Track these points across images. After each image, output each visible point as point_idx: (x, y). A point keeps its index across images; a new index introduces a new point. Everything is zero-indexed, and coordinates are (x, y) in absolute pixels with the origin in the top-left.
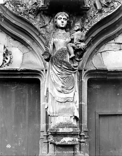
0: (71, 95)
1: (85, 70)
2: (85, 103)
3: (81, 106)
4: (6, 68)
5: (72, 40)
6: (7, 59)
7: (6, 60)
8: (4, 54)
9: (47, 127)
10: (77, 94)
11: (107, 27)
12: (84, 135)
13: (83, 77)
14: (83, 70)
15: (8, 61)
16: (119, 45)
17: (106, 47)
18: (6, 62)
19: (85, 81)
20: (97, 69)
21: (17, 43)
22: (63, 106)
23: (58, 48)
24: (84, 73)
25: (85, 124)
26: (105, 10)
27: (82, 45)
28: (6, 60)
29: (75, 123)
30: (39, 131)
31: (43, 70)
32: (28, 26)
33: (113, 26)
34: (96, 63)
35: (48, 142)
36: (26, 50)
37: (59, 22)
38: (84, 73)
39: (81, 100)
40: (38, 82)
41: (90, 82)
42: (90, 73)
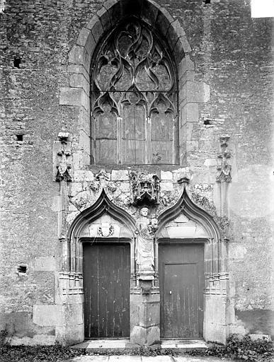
0: (150, 253)
2: (157, 257)
4: (111, 236)
5: (151, 223)
11: (86, 305)
17: (170, 224)
19: (157, 244)
21: (117, 222)
22: (146, 259)
23: (143, 228)
25: (157, 269)
26: (168, 204)
27: (156, 226)
29: (152, 269)
30: (130, 274)
33: (195, 214)
34: (164, 234)
36: (122, 226)
37: (143, 214)
38: (156, 240)
40: (129, 244)
42: (160, 240)
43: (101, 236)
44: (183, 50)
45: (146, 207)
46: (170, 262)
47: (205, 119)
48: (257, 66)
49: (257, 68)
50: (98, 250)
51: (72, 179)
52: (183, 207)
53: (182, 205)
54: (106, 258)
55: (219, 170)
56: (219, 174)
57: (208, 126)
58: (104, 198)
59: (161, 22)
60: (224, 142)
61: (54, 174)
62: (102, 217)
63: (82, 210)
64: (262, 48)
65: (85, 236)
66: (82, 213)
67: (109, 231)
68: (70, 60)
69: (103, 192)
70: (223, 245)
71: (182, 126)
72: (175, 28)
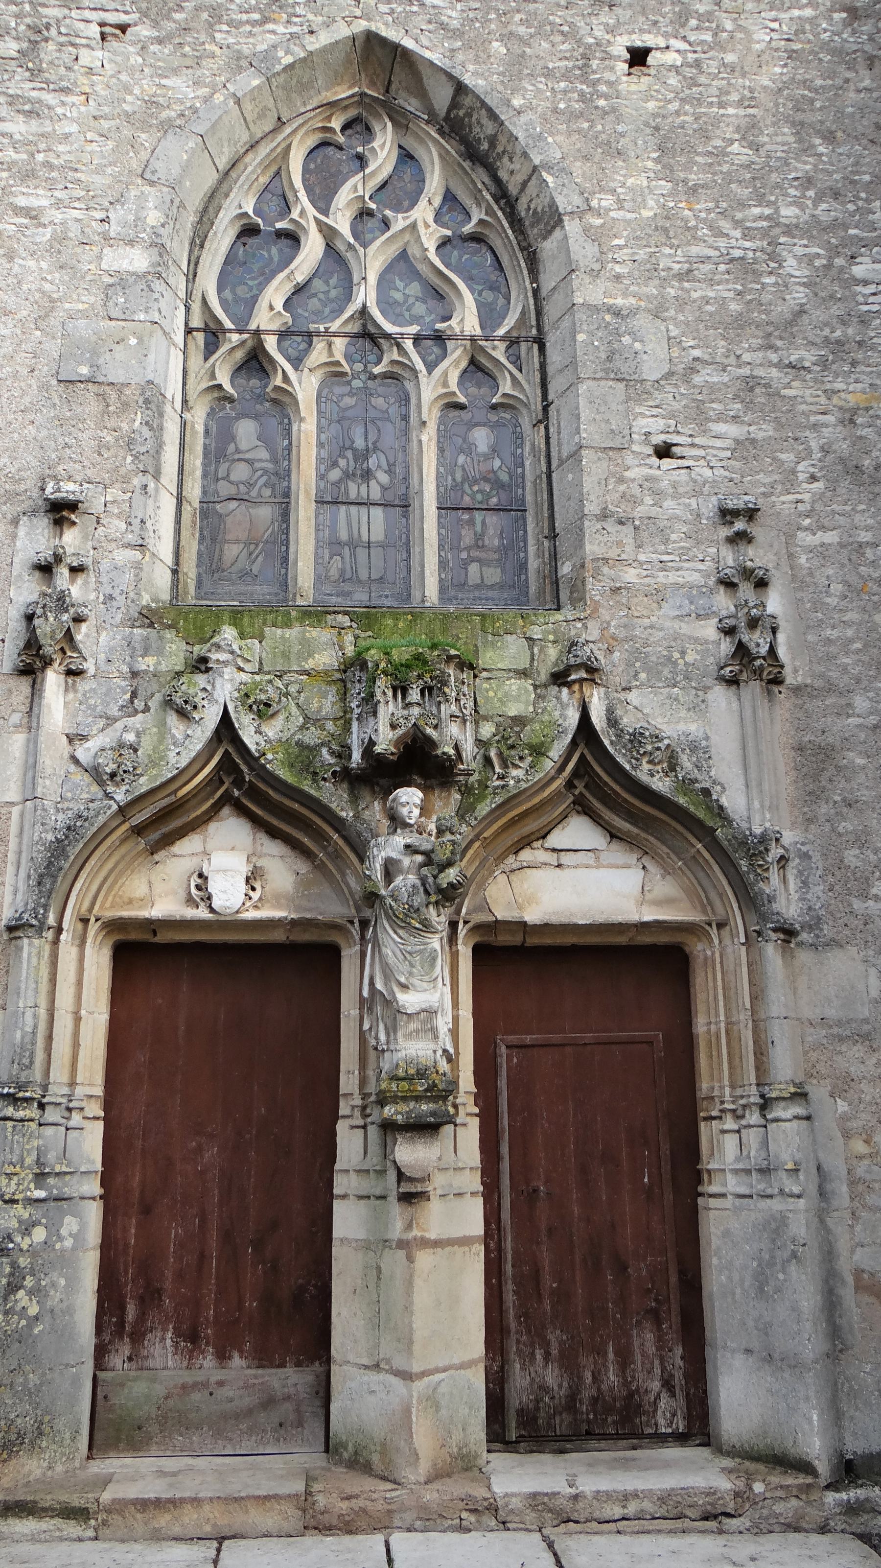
1: (465, 922)
3: (456, 1019)
6: (253, 889)
7: (251, 893)
8: (248, 880)
9: (363, 1082)
10: (447, 990)
12: (464, 1104)
13: (460, 942)
14: (93, 919)
15: (255, 896)
16: (555, 855)
18: (250, 898)
19: (465, 952)
20: (499, 918)
24: (464, 932)
28: (251, 893)
31: (710, 925)
32: (146, 802)
33: (631, 815)
35: (364, 1127)
38: (462, 931)
39: (455, 1004)
41: (479, 952)
42: (113, 926)
43: (202, 913)
44: (553, 205)
45: (418, 786)
46: (644, 1045)
47: (658, 439)
48: (839, 261)
49: (842, 269)
50: (819, 1298)
51: (89, 666)
52: (580, 788)
53: (575, 774)
54: (525, 1399)
55: (730, 631)
56: (726, 647)
57: (667, 463)
58: (225, 746)
59: (469, 115)
60: (740, 525)
61: (509, 1519)
62: (213, 827)
63: (121, 796)
64: (851, 207)
65: (125, 914)
66: (123, 811)
67: (242, 887)
68: (114, 229)
69: (226, 721)
70: (771, 951)
71: (561, 462)
72: (521, 135)
